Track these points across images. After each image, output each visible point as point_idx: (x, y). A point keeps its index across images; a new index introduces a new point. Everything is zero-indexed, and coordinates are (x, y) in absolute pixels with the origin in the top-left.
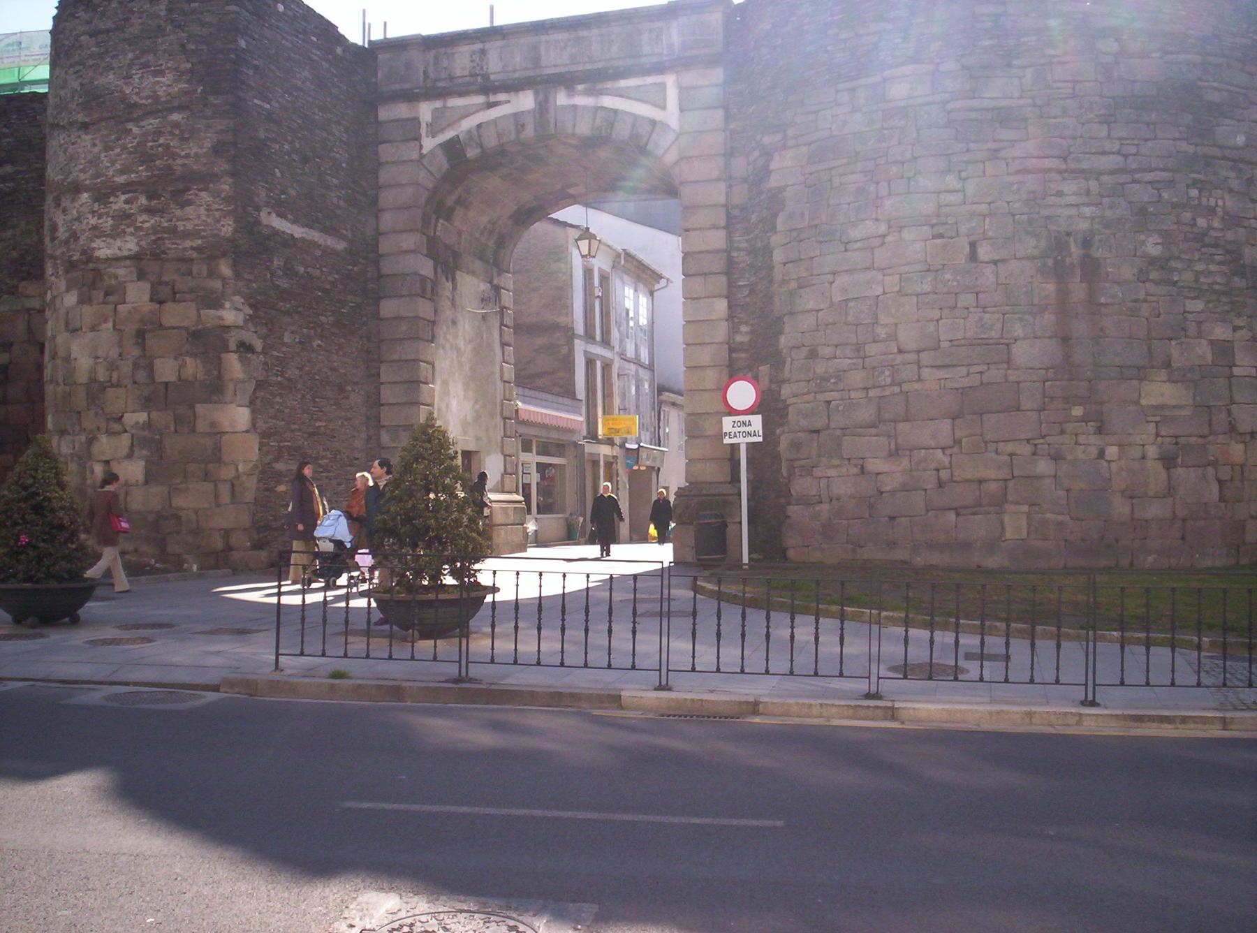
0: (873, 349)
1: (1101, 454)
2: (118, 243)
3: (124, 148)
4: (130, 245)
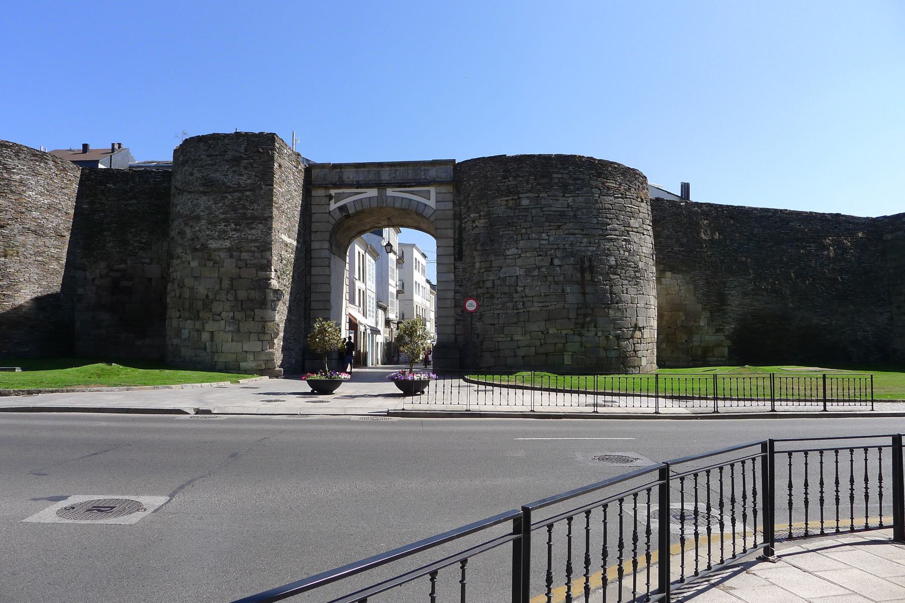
0: (515, 295)
1: (596, 335)
2: (221, 242)
3: (224, 204)
4: (227, 244)
